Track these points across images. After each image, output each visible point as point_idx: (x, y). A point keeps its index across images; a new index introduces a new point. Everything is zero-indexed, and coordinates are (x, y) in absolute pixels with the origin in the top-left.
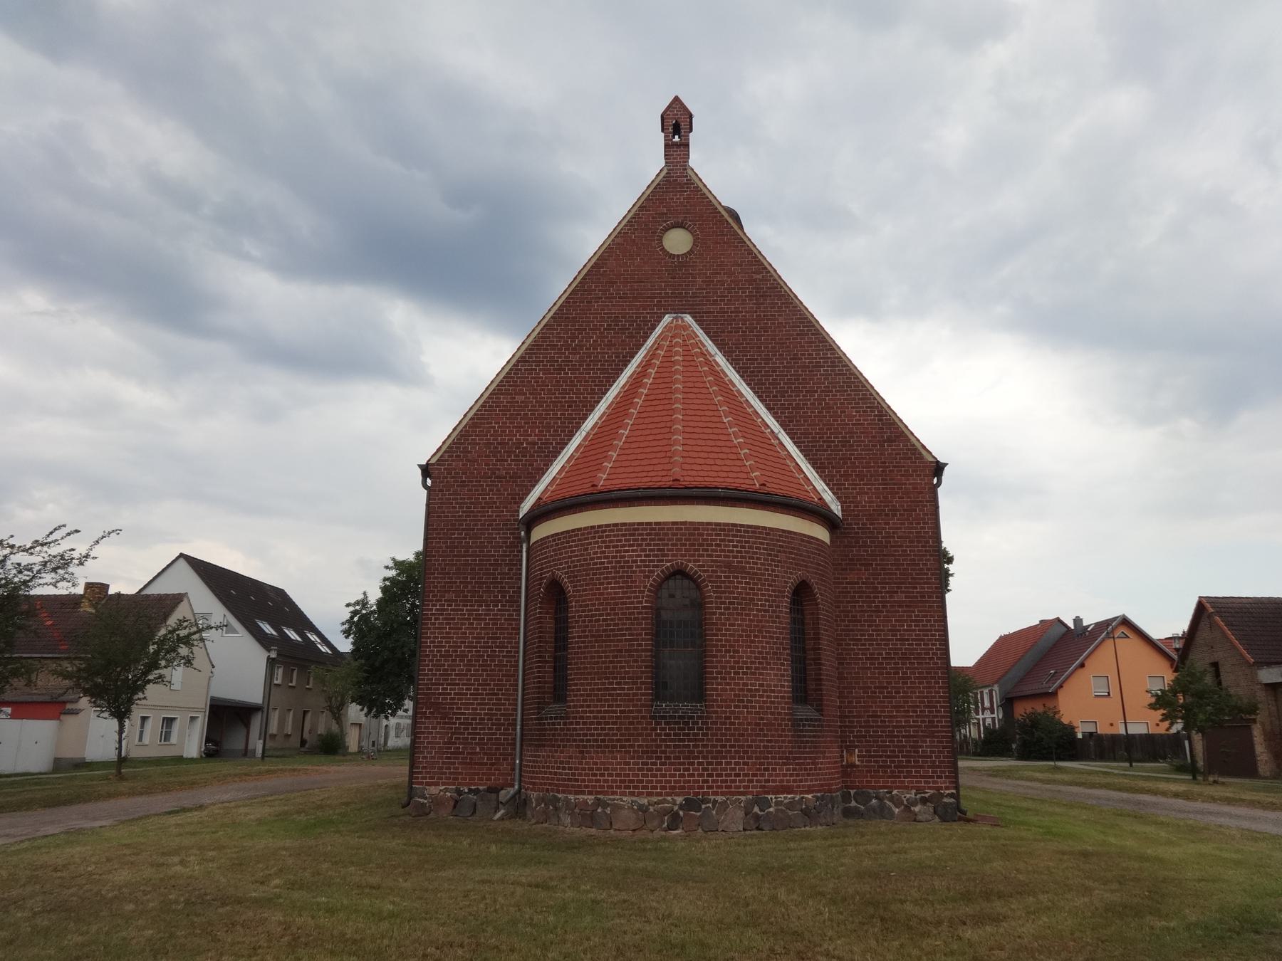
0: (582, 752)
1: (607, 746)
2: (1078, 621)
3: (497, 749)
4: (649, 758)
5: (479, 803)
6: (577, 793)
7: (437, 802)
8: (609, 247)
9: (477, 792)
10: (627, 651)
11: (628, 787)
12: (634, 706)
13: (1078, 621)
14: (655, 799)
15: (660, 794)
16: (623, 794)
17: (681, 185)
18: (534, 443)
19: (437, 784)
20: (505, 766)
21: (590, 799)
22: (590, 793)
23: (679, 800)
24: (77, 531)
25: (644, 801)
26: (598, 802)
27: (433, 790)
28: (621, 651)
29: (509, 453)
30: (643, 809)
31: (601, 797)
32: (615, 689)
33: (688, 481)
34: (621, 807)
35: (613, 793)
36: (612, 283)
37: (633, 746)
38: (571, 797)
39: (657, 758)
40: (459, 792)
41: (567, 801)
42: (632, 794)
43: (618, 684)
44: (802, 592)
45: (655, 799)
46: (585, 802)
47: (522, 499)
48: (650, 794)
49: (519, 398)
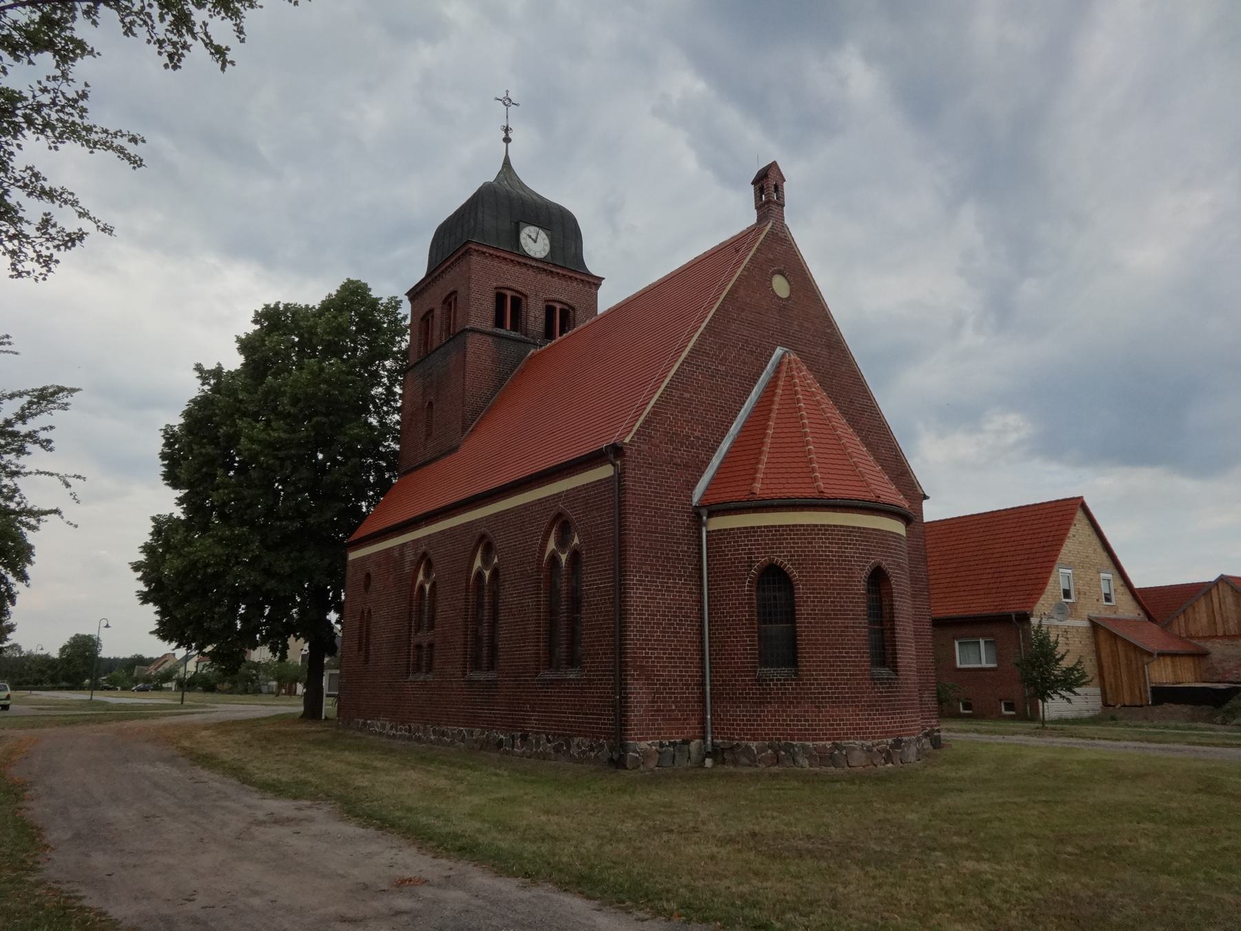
5: (677, 754)
6: (814, 740)
7: (646, 755)
9: (674, 744)
14: (876, 741)
15: (879, 738)
16: (856, 739)
17: (781, 239)
18: (698, 438)
19: (646, 739)
21: (829, 744)
22: (828, 739)
23: (890, 741)
24: (52, 428)
25: (869, 743)
26: (836, 746)
27: (644, 745)
29: (682, 444)
30: (869, 750)
33: (829, 493)
34: (854, 749)
36: (743, 310)
38: (810, 744)
40: (661, 745)
41: (804, 747)
42: (862, 738)
44: (878, 578)
45: (876, 741)
46: (824, 746)
47: (694, 486)
48: (874, 738)
49: (687, 395)
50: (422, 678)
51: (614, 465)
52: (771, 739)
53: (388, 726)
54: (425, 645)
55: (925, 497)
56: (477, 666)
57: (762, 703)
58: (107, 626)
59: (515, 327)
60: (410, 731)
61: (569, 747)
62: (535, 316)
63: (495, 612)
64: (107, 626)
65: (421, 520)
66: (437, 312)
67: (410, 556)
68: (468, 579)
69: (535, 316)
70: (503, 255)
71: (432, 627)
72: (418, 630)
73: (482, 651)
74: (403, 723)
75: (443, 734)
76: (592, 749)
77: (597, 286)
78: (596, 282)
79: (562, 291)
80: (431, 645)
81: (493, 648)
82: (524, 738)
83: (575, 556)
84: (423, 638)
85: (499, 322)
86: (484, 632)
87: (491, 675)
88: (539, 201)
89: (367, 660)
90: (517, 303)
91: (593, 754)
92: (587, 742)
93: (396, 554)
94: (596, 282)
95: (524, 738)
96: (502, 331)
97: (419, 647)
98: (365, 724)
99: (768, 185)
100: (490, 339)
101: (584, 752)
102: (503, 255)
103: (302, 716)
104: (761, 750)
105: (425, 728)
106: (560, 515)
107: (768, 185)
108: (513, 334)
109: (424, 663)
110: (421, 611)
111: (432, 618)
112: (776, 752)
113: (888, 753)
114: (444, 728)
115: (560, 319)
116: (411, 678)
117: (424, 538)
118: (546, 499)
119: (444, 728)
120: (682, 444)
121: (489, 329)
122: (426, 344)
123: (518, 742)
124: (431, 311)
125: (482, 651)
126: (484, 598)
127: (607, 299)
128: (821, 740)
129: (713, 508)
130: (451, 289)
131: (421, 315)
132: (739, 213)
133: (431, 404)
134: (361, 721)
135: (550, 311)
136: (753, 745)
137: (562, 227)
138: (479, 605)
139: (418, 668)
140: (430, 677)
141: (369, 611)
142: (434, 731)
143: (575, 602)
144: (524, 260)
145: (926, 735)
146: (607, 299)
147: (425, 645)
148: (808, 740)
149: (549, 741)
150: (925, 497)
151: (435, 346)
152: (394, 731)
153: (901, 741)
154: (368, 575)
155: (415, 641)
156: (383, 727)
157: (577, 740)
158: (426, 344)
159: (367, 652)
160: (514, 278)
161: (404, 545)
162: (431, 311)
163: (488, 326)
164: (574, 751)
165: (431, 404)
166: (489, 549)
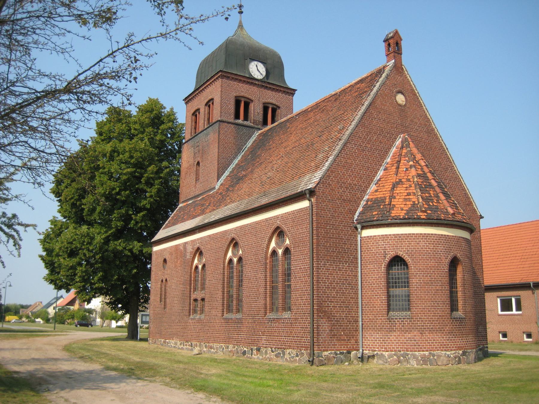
0: (421, 333)
1: (434, 331)
2: (59, 206)
3: (350, 333)
4: (451, 335)
6: (419, 351)
8: (437, 138)
10: (441, 290)
11: (443, 348)
12: (445, 313)
13: (59, 206)
15: (454, 350)
16: (442, 350)
19: (327, 351)
20: (353, 341)
21: (427, 353)
22: (427, 351)
24: (33, 209)
27: (326, 353)
28: (438, 290)
31: (432, 352)
32: (436, 306)
34: (441, 356)
35: (438, 350)
37: (444, 330)
39: (454, 335)
40: (336, 354)
43: (438, 304)
48: (451, 350)
50: (198, 317)
51: (310, 200)
52: (395, 351)
53: (179, 343)
54: (199, 299)
55: (482, 217)
56: (229, 310)
57: (390, 331)
58: (10, 286)
59: (246, 118)
60: (192, 346)
61: (284, 354)
62: (256, 110)
63: (240, 281)
64: (10, 286)
65: (196, 229)
66: (202, 111)
67: (190, 249)
68: (224, 262)
69: (256, 110)
70: (239, 78)
71: (203, 288)
72: (195, 290)
73: (232, 302)
74: (187, 341)
75: (211, 348)
76: (297, 356)
77: (293, 94)
78: (291, 92)
79: (272, 97)
80: (203, 300)
81: (239, 301)
82: (258, 350)
83: (287, 251)
84: (198, 295)
85: (237, 116)
86: (234, 291)
87: (239, 316)
88: (257, 45)
89: (165, 308)
90: (247, 105)
91: (297, 358)
92: (295, 352)
93: (181, 248)
94: (291, 92)
95: (258, 350)
96: (240, 121)
97: (196, 300)
98: (165, 342)
99: (394, 45)
100: (233, 126)
101: (293, 357)
102: (239, 78)
103: (127, 338)
104: (390, 356)
105: (200, 345)
106: (278, 228)
107: (394, 45)
108: (245, 123)
109: (198, 309)
110: (196, 281)
111: (203, 284)
112: (399, 357)
113: (459, 358)
114: (211, 344)
115: (270, 112)
116: (191, 317)
117: (198, 239)
118: (270, 219)
119: (211, 344)
120: (347, 188)
121: (232, 120)
122: (195, 128)
123: (255, 352)
124: (198, 110)
125: (232, 302)
126: (234, 273)
127: (300, 103)
128: (423, 351)
129: (364, 224)
130: (210, 98)
131: (192, 111)
132: (378, 59)
133: (198, 163)
134: (163, 340)
135: (265, 109)
136: (386, 354)
137: (274, 65)
138: (231, 277)
139: (195, 311)
140: (203, 316)
141: (166, 280)
142: (206, 346)
143: (288, 275)
144: (251, 80)
145: (480, 350)
146: (300, 103)
147: (199, 299)
148: (416, 351)
149: (273, 352)
150: (482, 217)
151: (200, 130)
152: (182, 346)
153: (466, 352)
154: (165, 261)
155: (193, 297)
156: (176, 344)
157: (288, 351)
158: (195, 128)
159: (165, 303)
160: (244, 90)
161: (186, 243)
162: (198, 110)
163: (231, 119)
164: (287, 356)
165: (198, 163)
166: (236, 245)
